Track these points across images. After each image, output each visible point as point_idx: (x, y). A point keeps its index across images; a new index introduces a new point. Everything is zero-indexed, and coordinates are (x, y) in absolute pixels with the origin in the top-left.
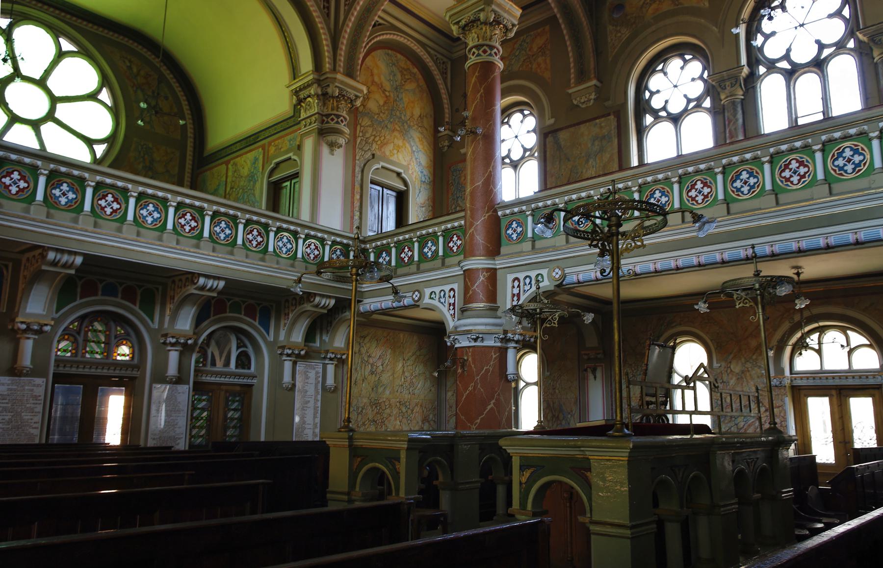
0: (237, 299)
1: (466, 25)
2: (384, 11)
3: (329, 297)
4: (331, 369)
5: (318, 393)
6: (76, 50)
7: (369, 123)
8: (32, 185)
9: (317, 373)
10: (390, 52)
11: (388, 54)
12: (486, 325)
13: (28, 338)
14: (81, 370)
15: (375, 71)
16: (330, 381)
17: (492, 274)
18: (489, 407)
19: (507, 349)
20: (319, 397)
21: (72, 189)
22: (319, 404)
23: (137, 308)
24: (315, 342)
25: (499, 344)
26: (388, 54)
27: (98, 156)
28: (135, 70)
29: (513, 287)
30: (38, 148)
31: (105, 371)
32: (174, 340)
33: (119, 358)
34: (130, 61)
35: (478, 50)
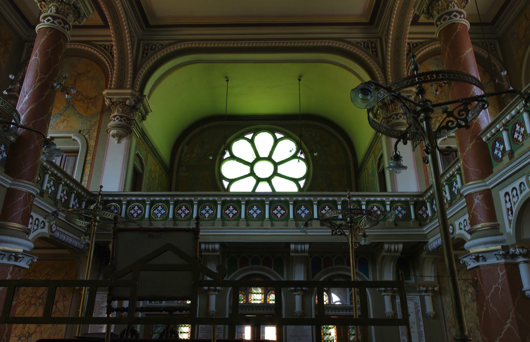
1: (428, 9)
2: (410, 33)
3: (398, 243)
4: (428, 299)
5: (420, 320)
6: (283, 136)
8: (191, 211)
9: (416, 304)
12: (485, 244)
13: (212, 294)
14: (258, 311)
16: (429, 309)
17: (488, 196)
18: (506, 327)
19: (517, 264)
20: (422, 323)
21: (306, 208)
22: (422, 329)
23: (272, 270)
24: (410, 279)
25: (503, 261)
27: (302, 186)
29: (506, 202)
30: (271, 191)
31: (262, 311)
32: (425, 289)
33: (252, 302)
35: (440, 21)
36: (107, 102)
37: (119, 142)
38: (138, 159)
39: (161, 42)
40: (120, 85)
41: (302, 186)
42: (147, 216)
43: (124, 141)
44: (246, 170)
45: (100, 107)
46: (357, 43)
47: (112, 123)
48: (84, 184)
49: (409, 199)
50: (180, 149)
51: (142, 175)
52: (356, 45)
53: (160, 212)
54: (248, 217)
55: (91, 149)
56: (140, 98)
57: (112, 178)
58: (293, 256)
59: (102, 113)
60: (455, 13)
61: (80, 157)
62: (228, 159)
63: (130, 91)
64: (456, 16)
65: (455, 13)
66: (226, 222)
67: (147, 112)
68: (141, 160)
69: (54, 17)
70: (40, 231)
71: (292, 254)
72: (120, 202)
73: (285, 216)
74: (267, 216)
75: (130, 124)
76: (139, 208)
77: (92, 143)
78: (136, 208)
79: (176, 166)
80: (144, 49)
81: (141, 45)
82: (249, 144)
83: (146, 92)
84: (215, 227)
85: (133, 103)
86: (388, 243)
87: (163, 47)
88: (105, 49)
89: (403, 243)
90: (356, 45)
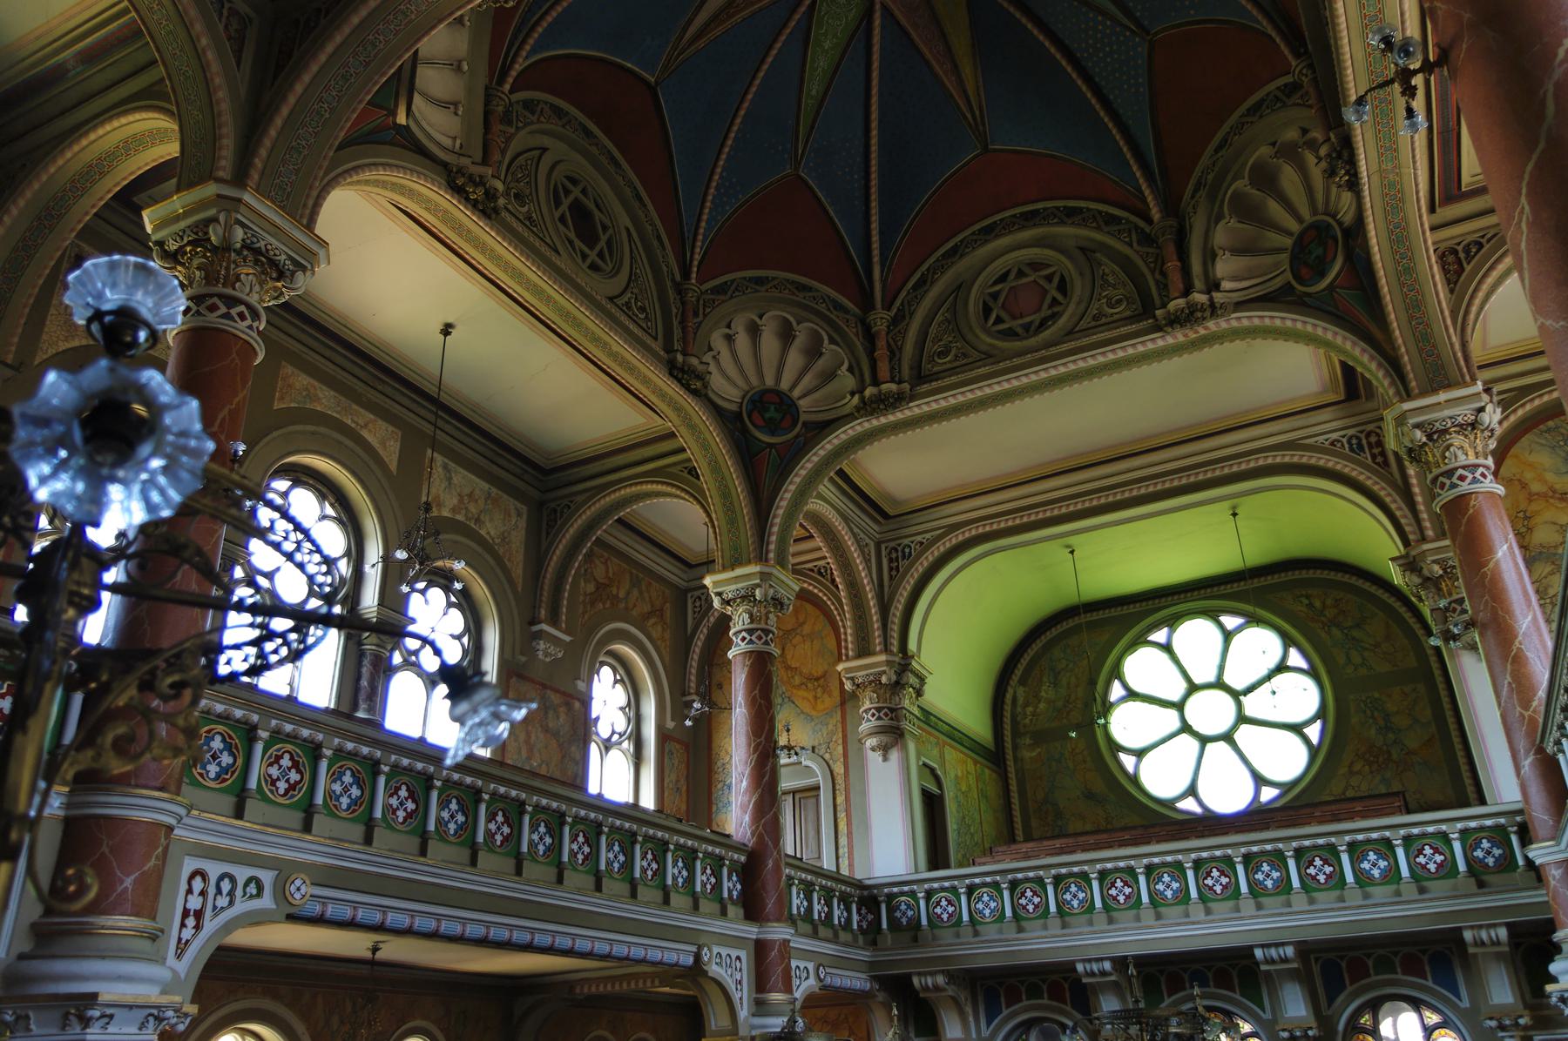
0: (1381, 952)
3: (1494, 926)
7: (1549, 568)
10: (1550, 424)
11: (1549, 430)
15: (1528, 475)
23: (1237, 996)
26: (1549, 430)
27: (1315, 740)
28: (1317, 604)
34: (1307, 597)
36: (848, 686)
37: (885, 759)
38: (927, 771)
39: (919, 538)
40: (864, 651)
41: (1315, 740)
42: (966, 917)
43: (894, 755)
44: (1171, 719)
45: (836, 693)
46: (1332, 444)
47: (864, 727)
48: (845, 871)
49: (1502, 821)
50: (1009, 696)
51: (941, 798)
52: (1332, 448)
53: (987, 905)
54: (1156, 900)
55: (840, 780)
56: (904, 664)
57: (888, 849)
58: (1268, 972)
59: (843, 703)
60: (1460, 472)
61: (825, 796)
62: (1123, 700)
63: (883, 658)
64: (1462, 478)
65: (1460, 472)
66: (1114, 914)
67: (922, 680)
68: (932, 770)
69: (750, 631)
70: (805, 985)
71: (1263, 967)
72: (913, 894)
73: (1230, 891)
74: (1194, 893)
75: (897, 719)
76: (950, 903)
77: (839, 769)
78: (944, 903)
79: (1009, 745)
80: (891, 561)
81: (884, 553)
82: (1164, 656)
83: (912, 645)
84: (1095, 928)
85: (894, 678)
86: (1472, 927)
87: (925, 547)
88: (820, 573)
89: (1508, 925)
90: (1332, 448)
